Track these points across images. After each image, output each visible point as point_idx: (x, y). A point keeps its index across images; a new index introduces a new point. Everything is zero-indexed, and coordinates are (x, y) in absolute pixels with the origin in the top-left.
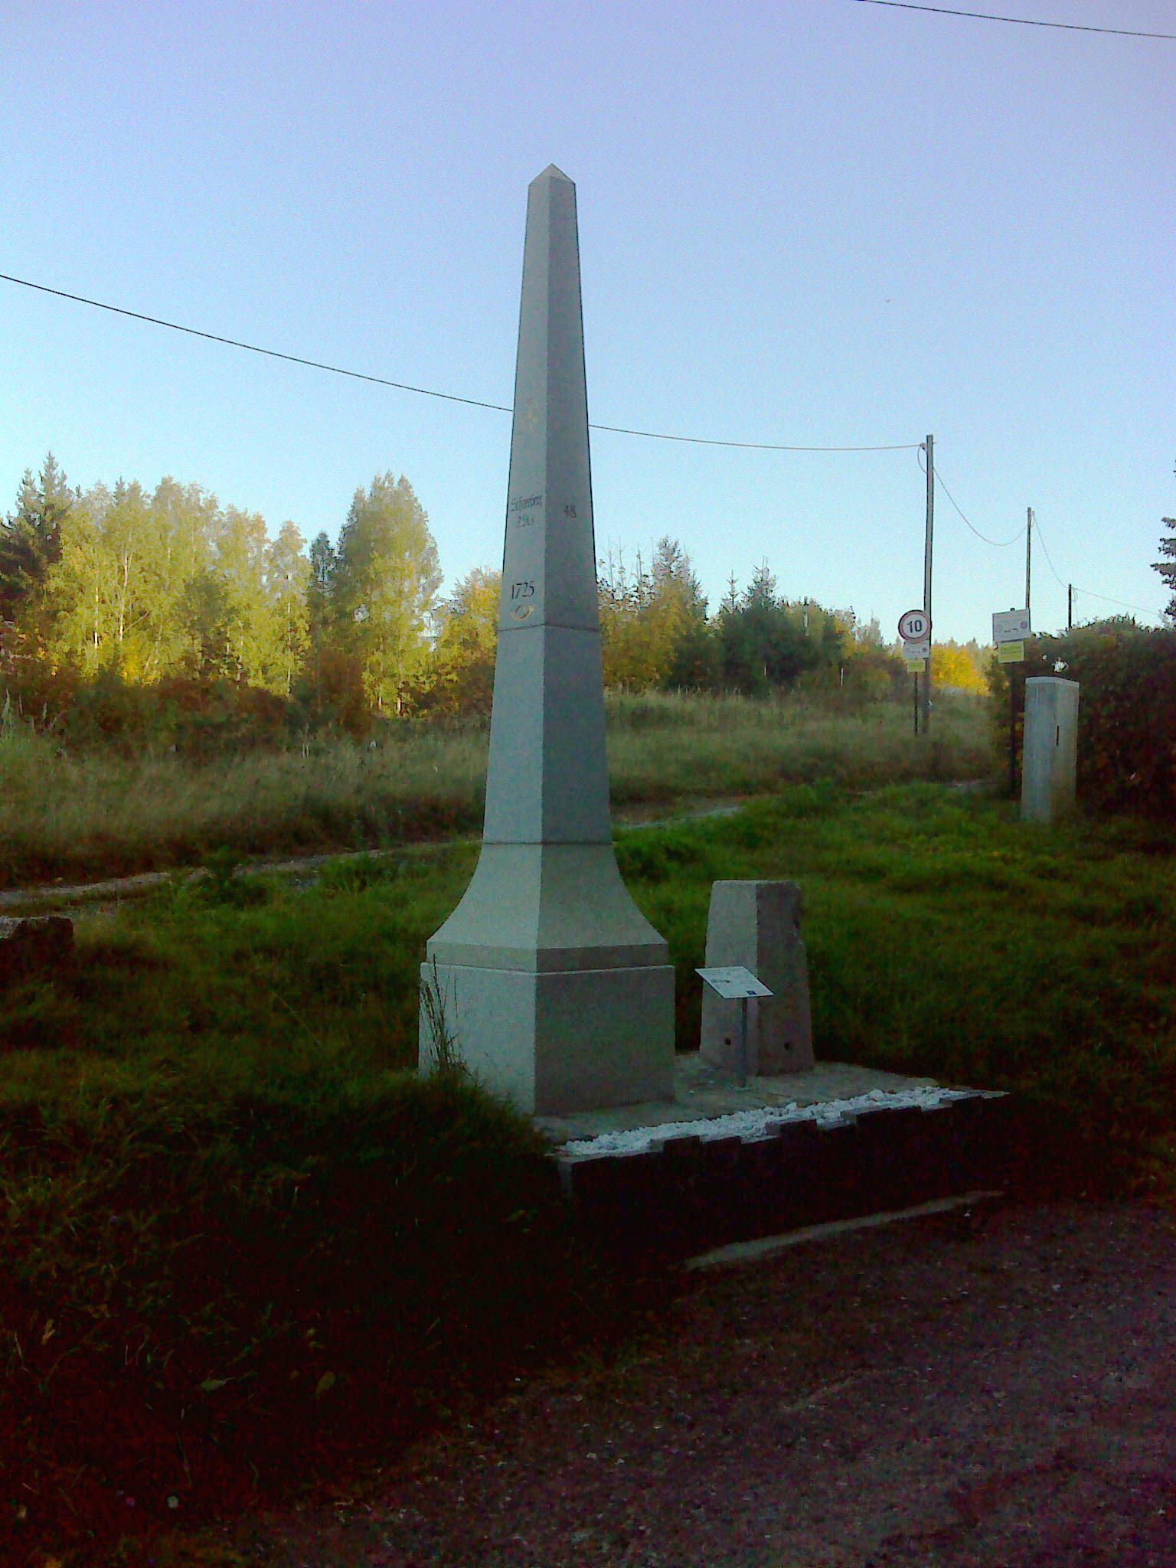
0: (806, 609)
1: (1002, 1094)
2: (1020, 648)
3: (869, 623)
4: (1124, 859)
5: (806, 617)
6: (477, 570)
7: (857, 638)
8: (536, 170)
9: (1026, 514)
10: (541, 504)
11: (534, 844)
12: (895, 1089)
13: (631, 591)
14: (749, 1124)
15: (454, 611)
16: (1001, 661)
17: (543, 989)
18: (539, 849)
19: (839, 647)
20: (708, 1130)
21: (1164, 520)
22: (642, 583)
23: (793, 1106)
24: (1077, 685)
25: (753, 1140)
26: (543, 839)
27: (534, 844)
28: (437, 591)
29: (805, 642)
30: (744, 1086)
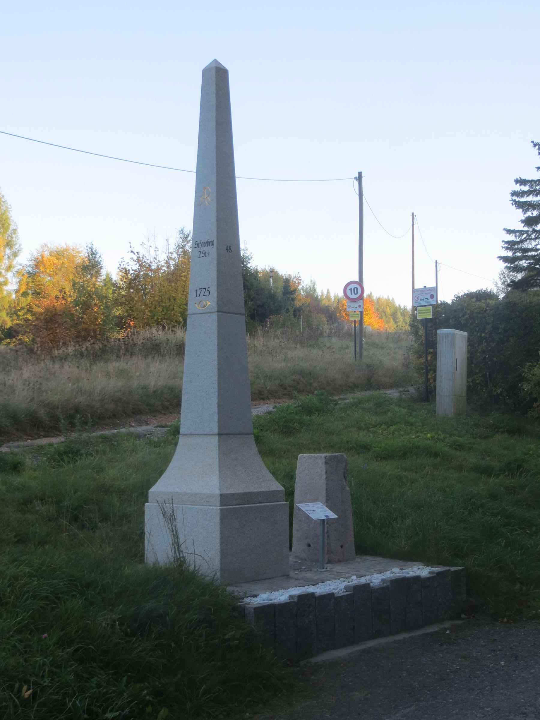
0: (271, 274)
1: (460, 568)
2: (429, 310)
3: (309, 284)
4: (498, 437)
5: (271, 280)
6: (45, 244)
7: (302, 292)
8: (206, 62)
9: (411, 217)
10: (213, 245)
11: (213, 435)
12: (404, 568)
13: (163, 263)
14: (336, 587)
15: (29, 273)
16: (419, 318)
17: (224, 516)
18: (217, 438)
19: (293, 300)
20: (319, 590)
21: (505, 229)
22: (169, 258)
23: (354, 577)
24: (465, 334)
25: (340, 595)
26: (219, 432)
27: (213, 435)
28: (18, 259)
29: (272, 297)
30: (323, 568)
